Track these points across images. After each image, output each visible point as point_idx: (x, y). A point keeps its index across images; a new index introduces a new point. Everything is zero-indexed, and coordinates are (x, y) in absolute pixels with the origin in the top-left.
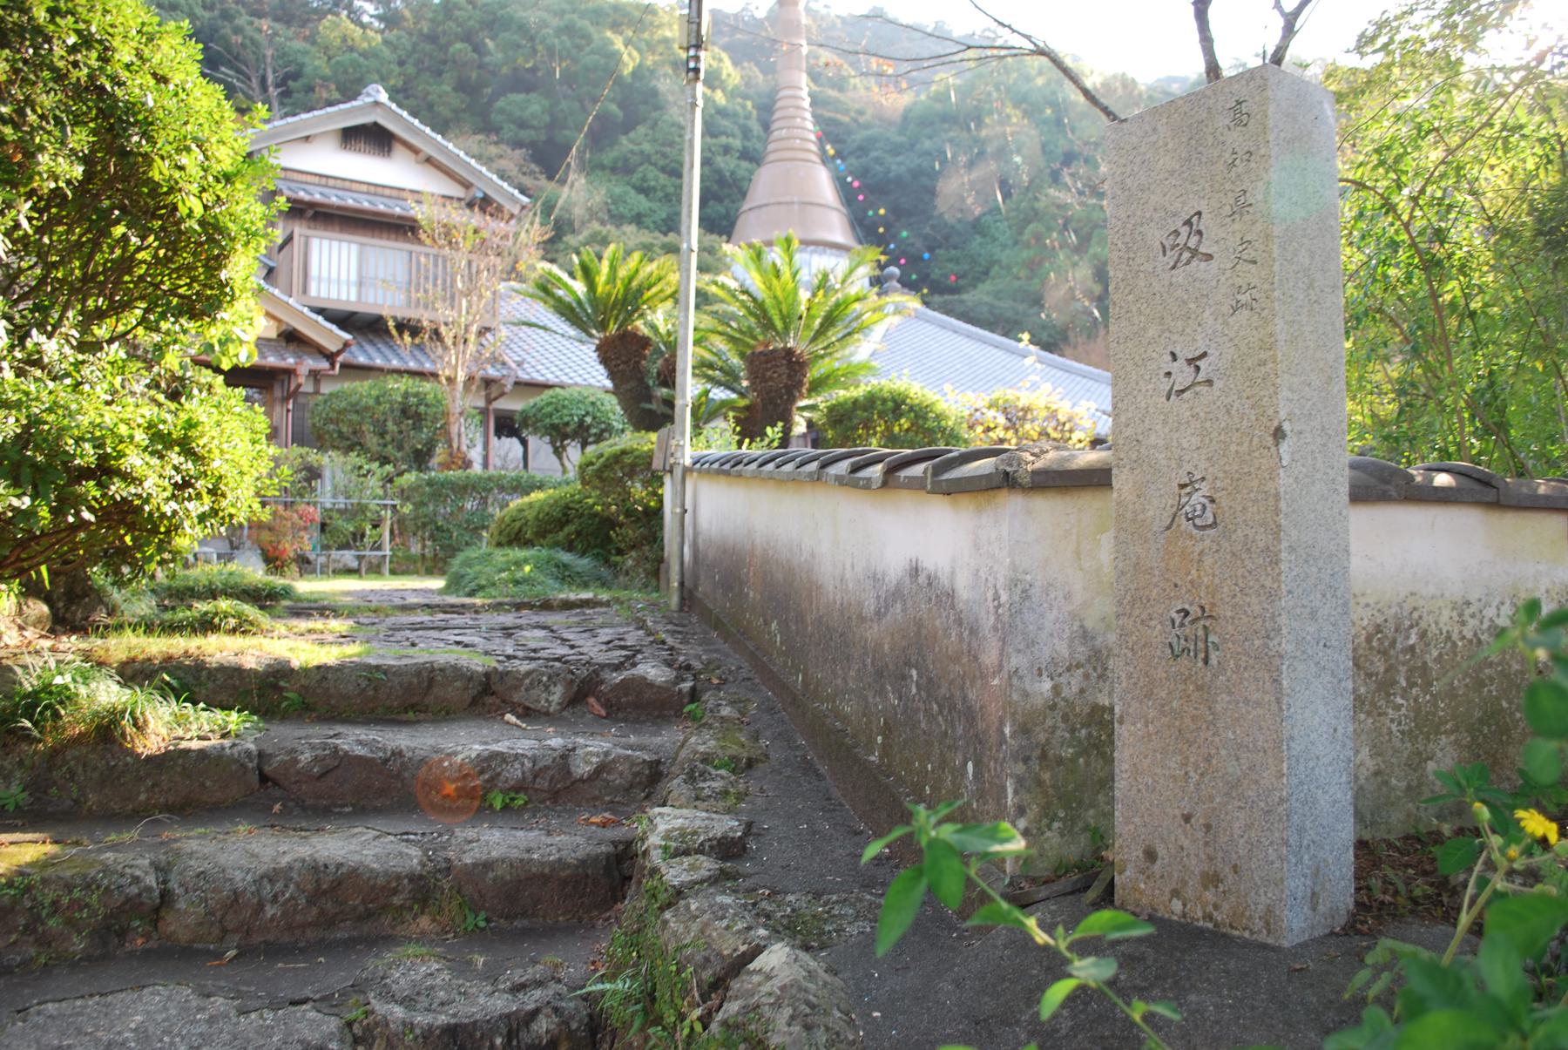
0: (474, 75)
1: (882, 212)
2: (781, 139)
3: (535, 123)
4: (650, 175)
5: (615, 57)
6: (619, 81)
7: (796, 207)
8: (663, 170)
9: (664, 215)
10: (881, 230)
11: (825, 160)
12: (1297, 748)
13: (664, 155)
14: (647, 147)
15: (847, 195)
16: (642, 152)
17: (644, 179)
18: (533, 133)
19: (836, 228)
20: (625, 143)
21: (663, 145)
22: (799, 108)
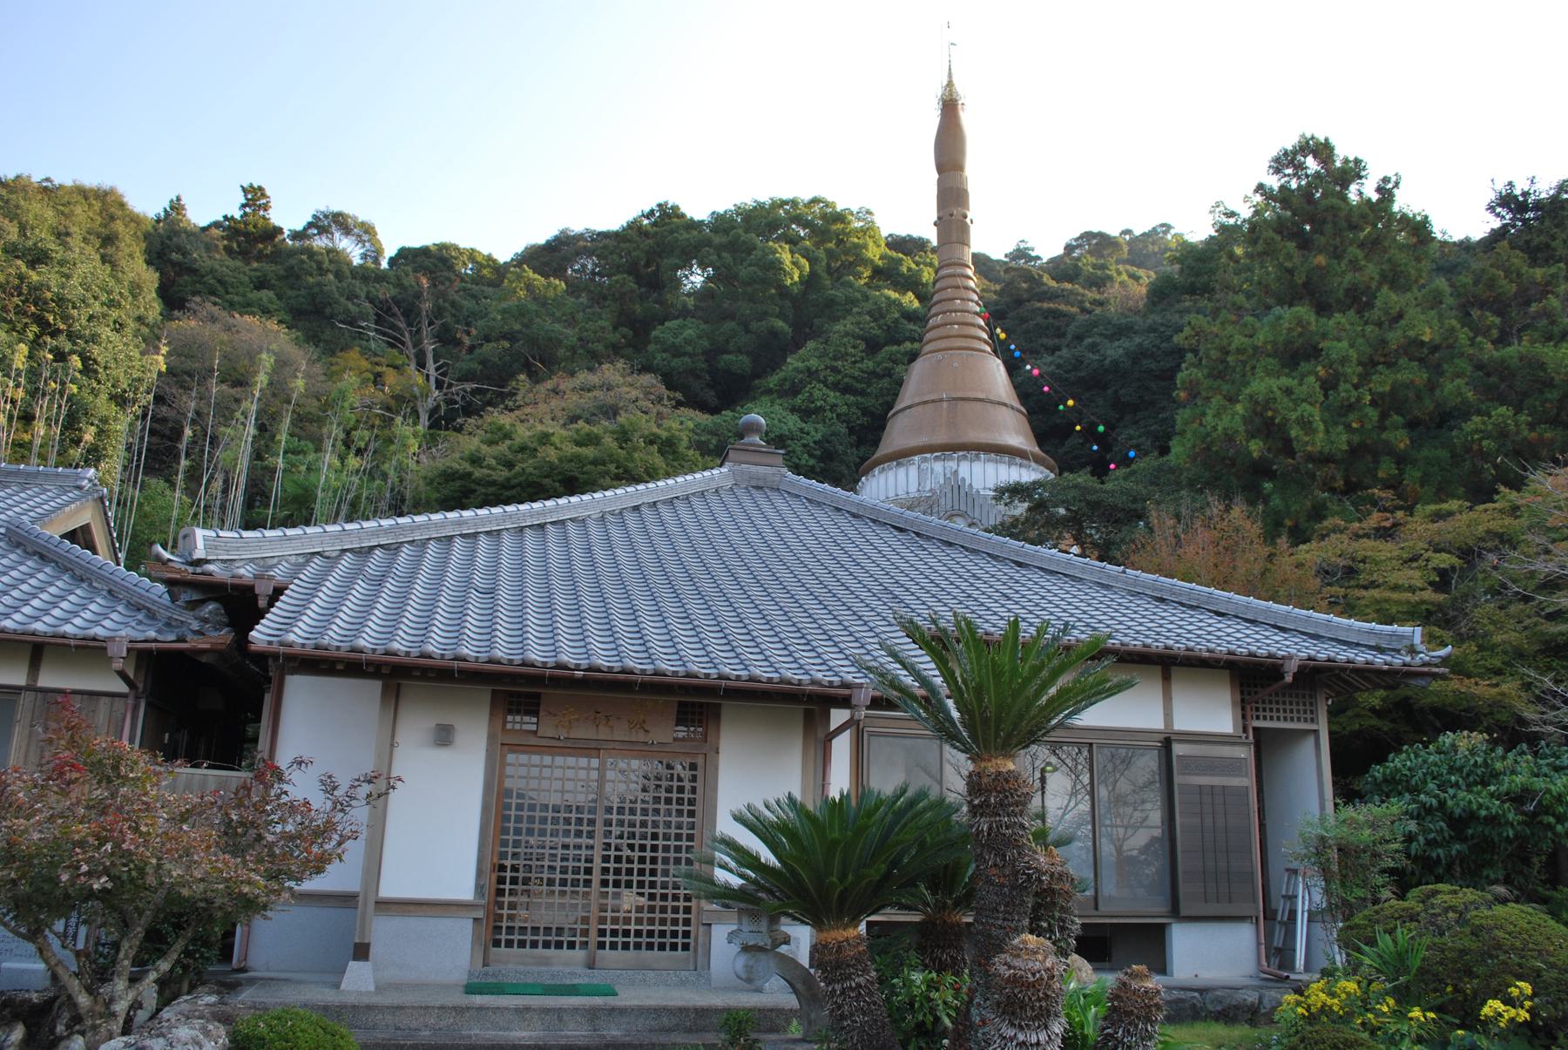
0: (638, 308)
1: (1070, 403)
2: (938, 326)
3: (689, 349)
4: (817, 394)
5: (776, 266)
6: (783, 291)
7: (945, 404)
8: (835, 386)
9: (818, 437)
10: (1101, 428)
11: (1000, 349)
12: (1471, 543)
13: (835, 370)
14: (814, 363)
15: (1026, 391)
16: (809, 369)
17: (811, 400)
18: (687, 359)
19: (1016, 434)
20: (793, 362)
21: (835, 359)
22: (967, 288)
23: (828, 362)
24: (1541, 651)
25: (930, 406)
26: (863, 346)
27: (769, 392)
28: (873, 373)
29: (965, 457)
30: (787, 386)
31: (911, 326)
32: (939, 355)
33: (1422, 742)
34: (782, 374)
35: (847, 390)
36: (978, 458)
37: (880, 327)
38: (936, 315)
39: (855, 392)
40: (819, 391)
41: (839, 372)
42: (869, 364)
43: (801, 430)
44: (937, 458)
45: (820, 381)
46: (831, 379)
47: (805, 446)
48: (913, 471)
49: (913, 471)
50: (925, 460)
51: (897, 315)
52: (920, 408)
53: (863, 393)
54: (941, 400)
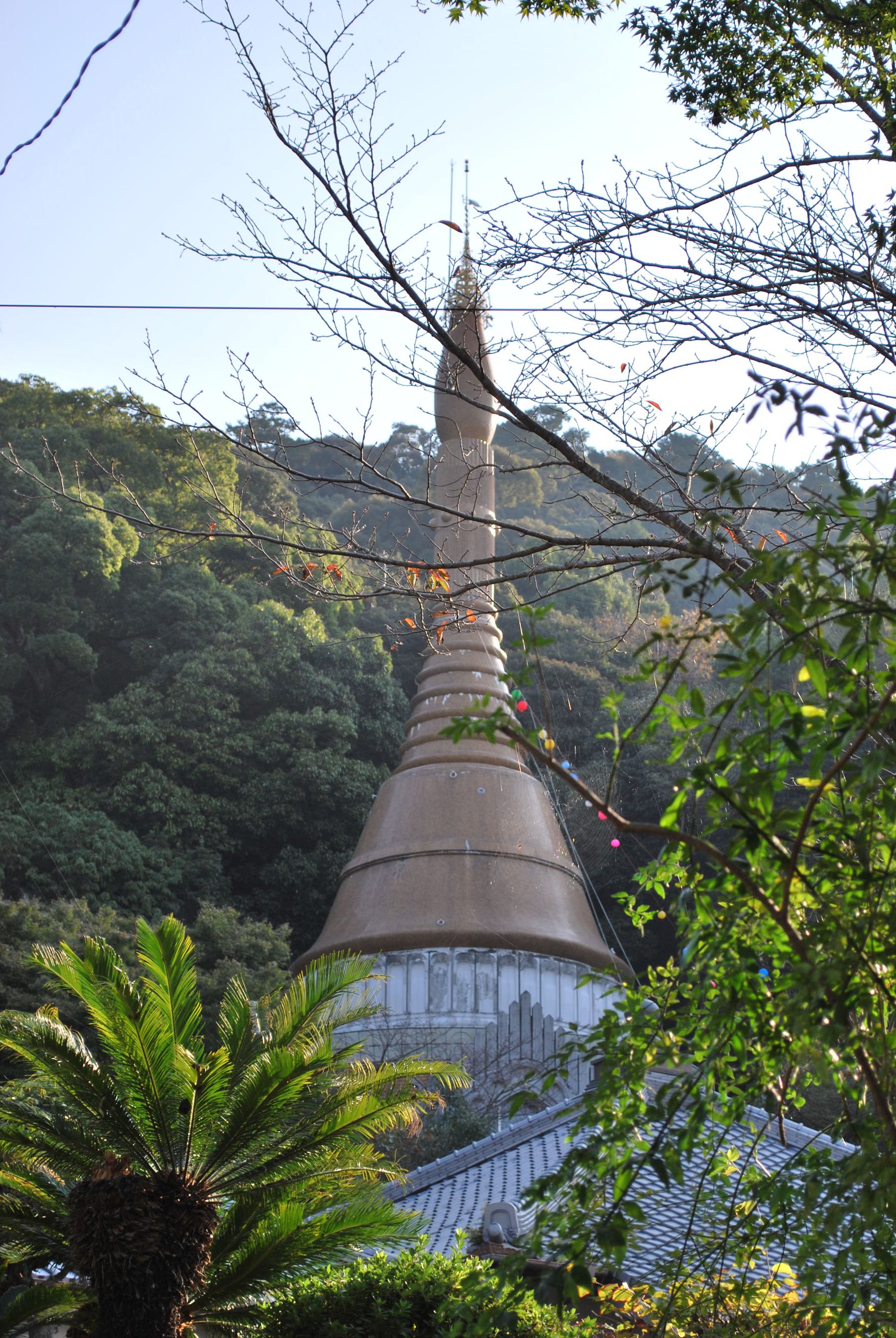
4: (152, 789)
7: (468, 861)
8: (181, 777)
9: (177, 876)
13: (186, 747)
16: (137, 739)
17: (139, 797)
21: (184, 724)
23: (171, 729)
24: (34, 940)
25: (440, 860)
26: (235, 707)
27: (48, 769)
28: (253, 759)
29: (510, 960)
30: (88, 763)
31: (321, 678)
32: (453, 769)
33: (286, 1268)
34: (78, 741)
35: (202, 785)
36: (531, 963)
37: (265, 673)
38: (441, 693)
39: (216, 790)
40: (157, 783)
41: (192, 751)
42: (246, 741)
43: (147, 863)
44: (462, 958)
45: (155, 765)
46: (178, 762)
47: (153, 891)
48: (419, 976)
49: (419, 976)
50: (443, 958)
51: (297, 655)
52: (423, 862)
53: (233, 794)
54: (461, 853)
